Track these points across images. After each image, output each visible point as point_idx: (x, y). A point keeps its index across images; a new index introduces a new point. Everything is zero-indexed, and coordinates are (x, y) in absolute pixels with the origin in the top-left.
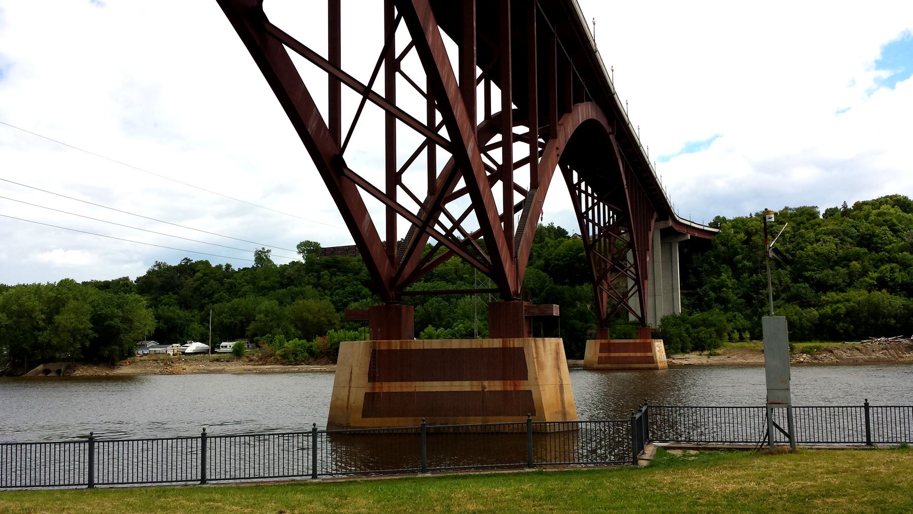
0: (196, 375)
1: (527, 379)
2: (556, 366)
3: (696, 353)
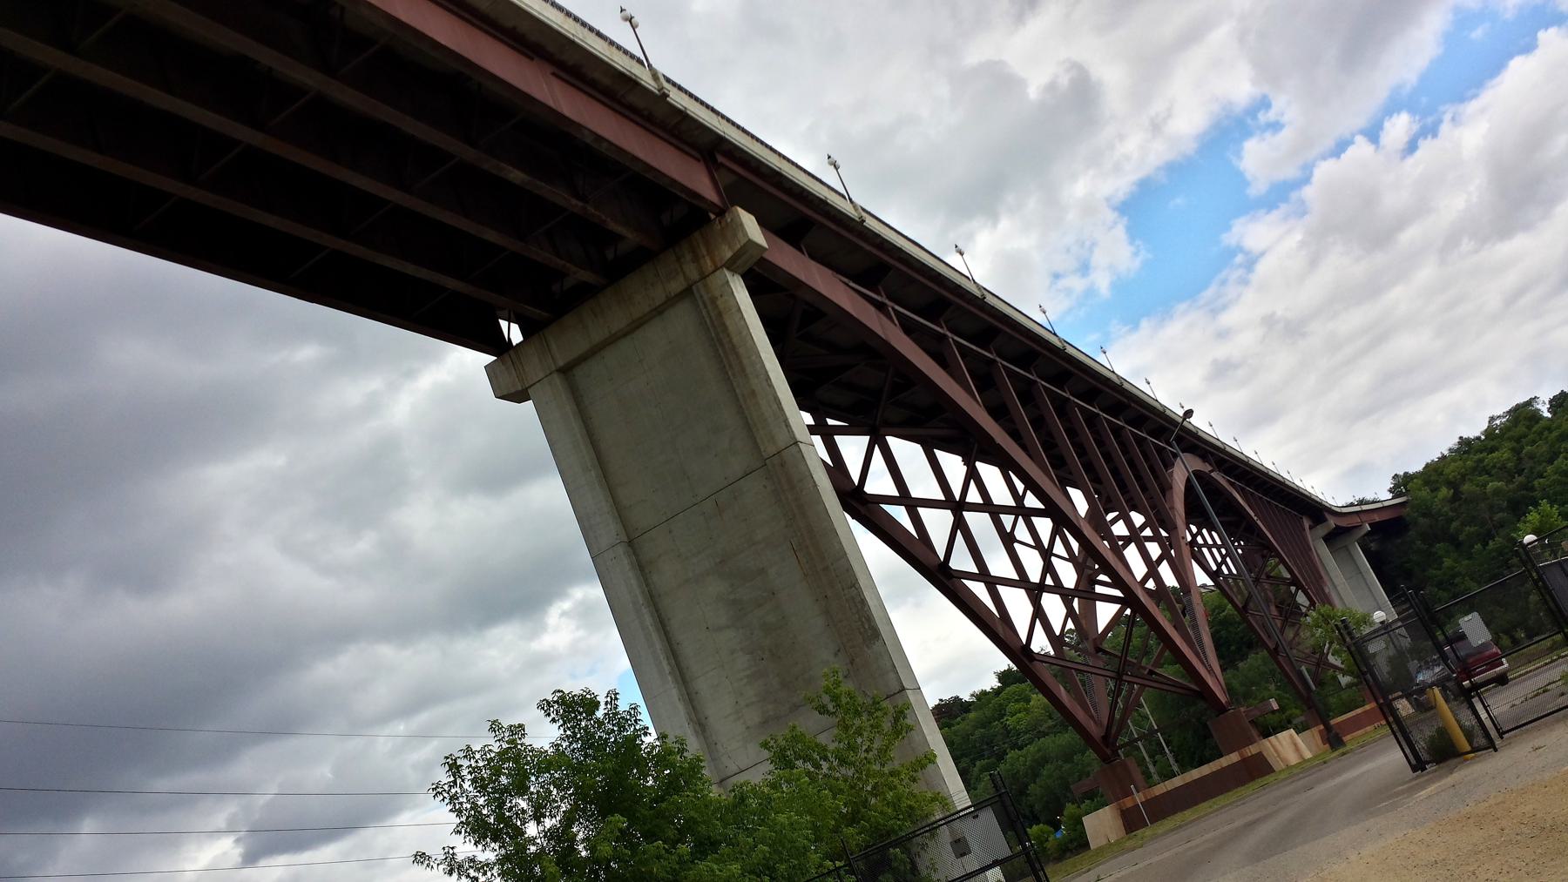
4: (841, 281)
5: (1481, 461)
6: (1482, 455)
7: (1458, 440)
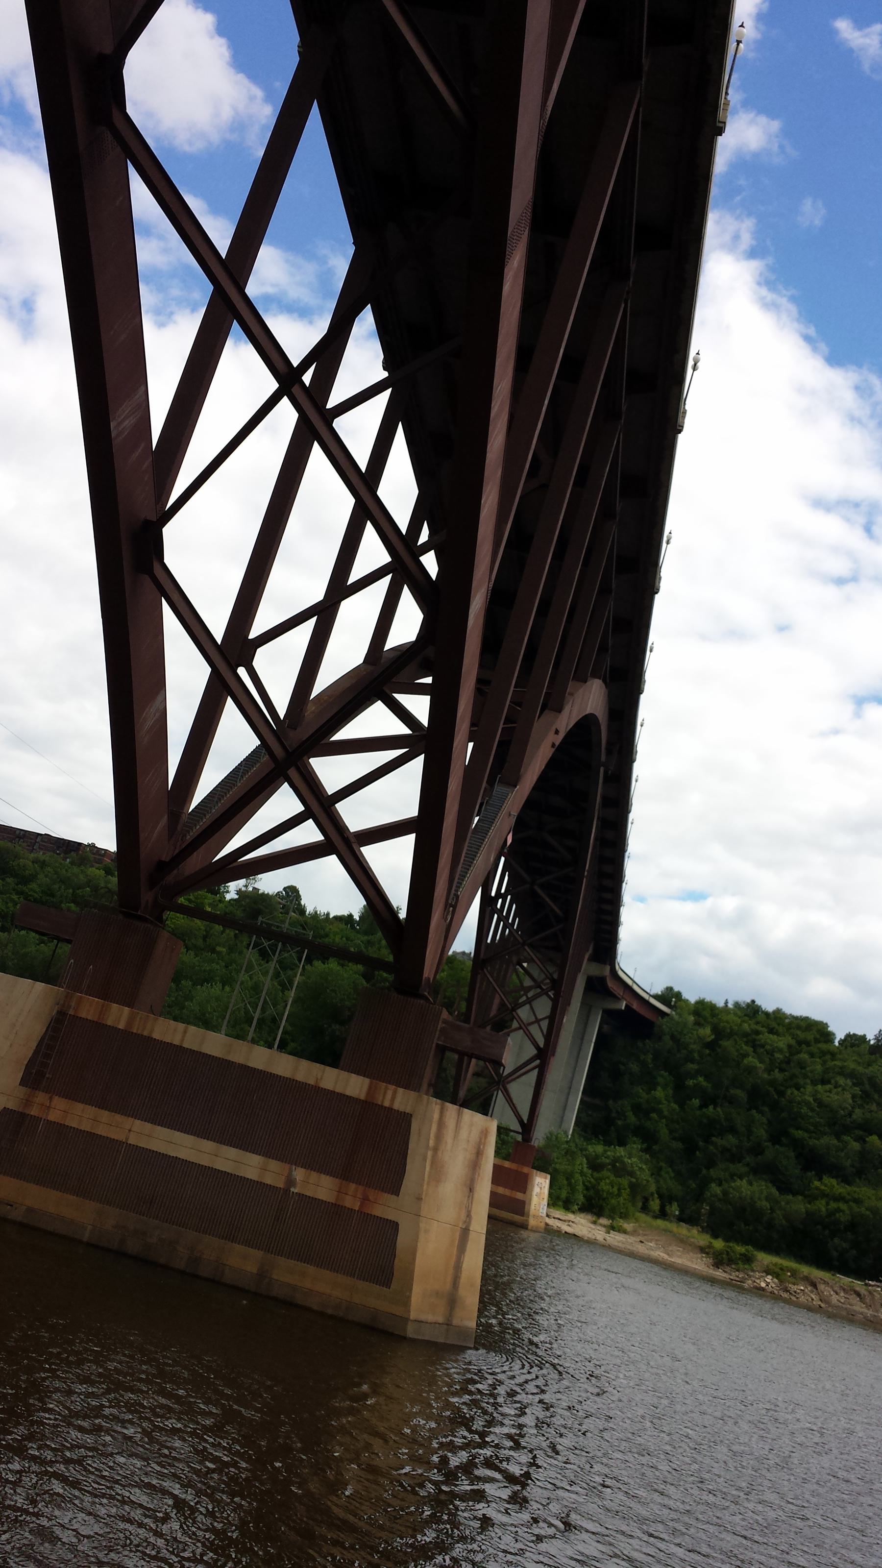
1: (397, 1193)
4: (539, 717)
5: (757, 1033)
6: (762, 1029)
7: (749, 1001)
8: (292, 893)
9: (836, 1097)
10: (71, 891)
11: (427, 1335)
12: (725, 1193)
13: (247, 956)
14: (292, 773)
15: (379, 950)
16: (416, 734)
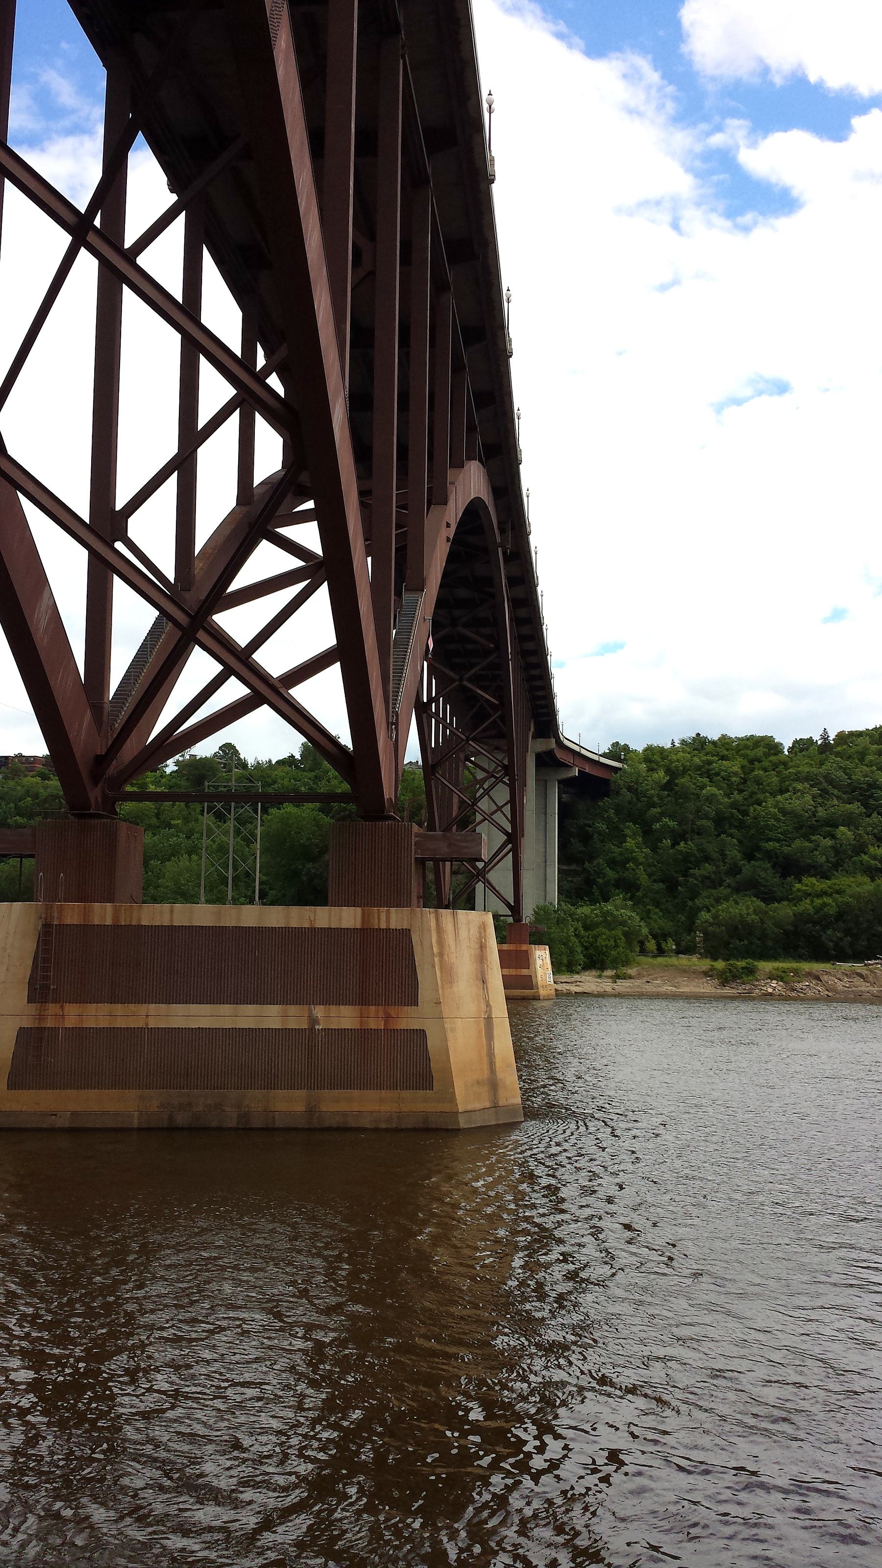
0: (16, 1126)
1: (414, 1002)
2: (480, 975)
3: (591, 974)
5: (710, 763)
8: (229, 749)
9: (798, 802)
10: (12, 805)
11: (478, 1121)
12: (715, 917)
13: (205, 822)
14: (201, 635)
15: (330, 782)
16: (309, 564)
